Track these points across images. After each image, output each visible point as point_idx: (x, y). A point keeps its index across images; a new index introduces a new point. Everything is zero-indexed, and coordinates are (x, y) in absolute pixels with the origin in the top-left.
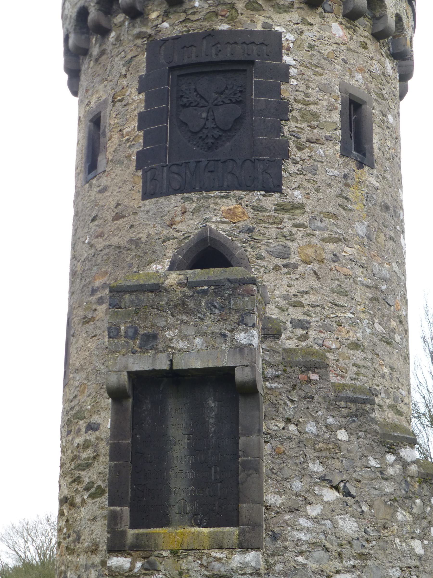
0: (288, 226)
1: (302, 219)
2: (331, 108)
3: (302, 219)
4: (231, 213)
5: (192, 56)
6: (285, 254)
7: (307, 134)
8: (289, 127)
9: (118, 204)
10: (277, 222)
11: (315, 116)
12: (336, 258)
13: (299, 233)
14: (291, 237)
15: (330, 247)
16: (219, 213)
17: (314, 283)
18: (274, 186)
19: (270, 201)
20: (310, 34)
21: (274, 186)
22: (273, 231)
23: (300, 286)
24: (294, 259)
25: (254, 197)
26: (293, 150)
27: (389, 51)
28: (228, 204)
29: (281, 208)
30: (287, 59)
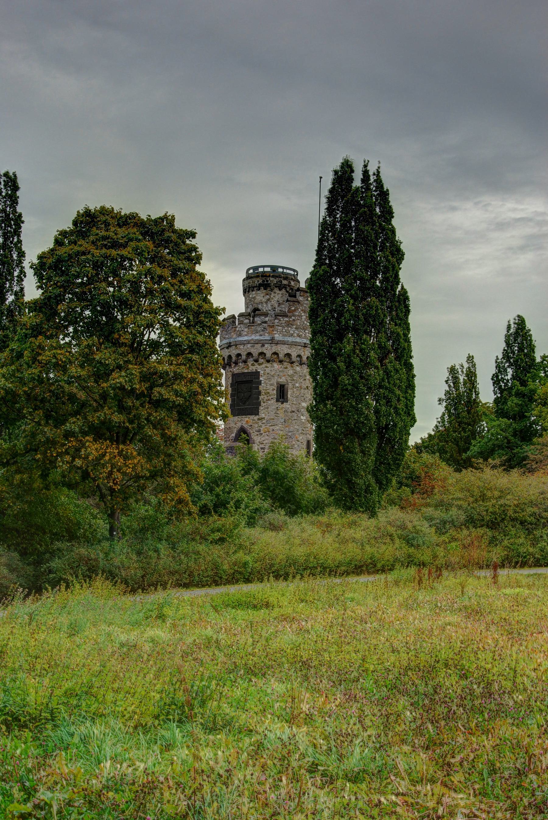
0: (260, 424)
1: (264, 421)
2: (273, 390)
3: (264, 421)
4: (247, 421)
5: (240, 379)
6: (259, 431)
7: (266, 398)
8: (261, 397)
9: (183, 709)
10: (257, 423)
11: (269, 393)
12: (273, 430)
13: (263, 425)
14: (261, 426)
15: (271, 427)
16: (245, 421)
17: (267, 437)
18: (257, 414)
19: (256, 418)
20: (268, 370)
21: (257, 414)
22: (256, 426)
23: (263, 439)
24: (262, 432)
25: (252, 417)
26: (262, 403)
27: (457, 390)
28: (247, 419)
29: (259, 419)
30: (261, 379)
